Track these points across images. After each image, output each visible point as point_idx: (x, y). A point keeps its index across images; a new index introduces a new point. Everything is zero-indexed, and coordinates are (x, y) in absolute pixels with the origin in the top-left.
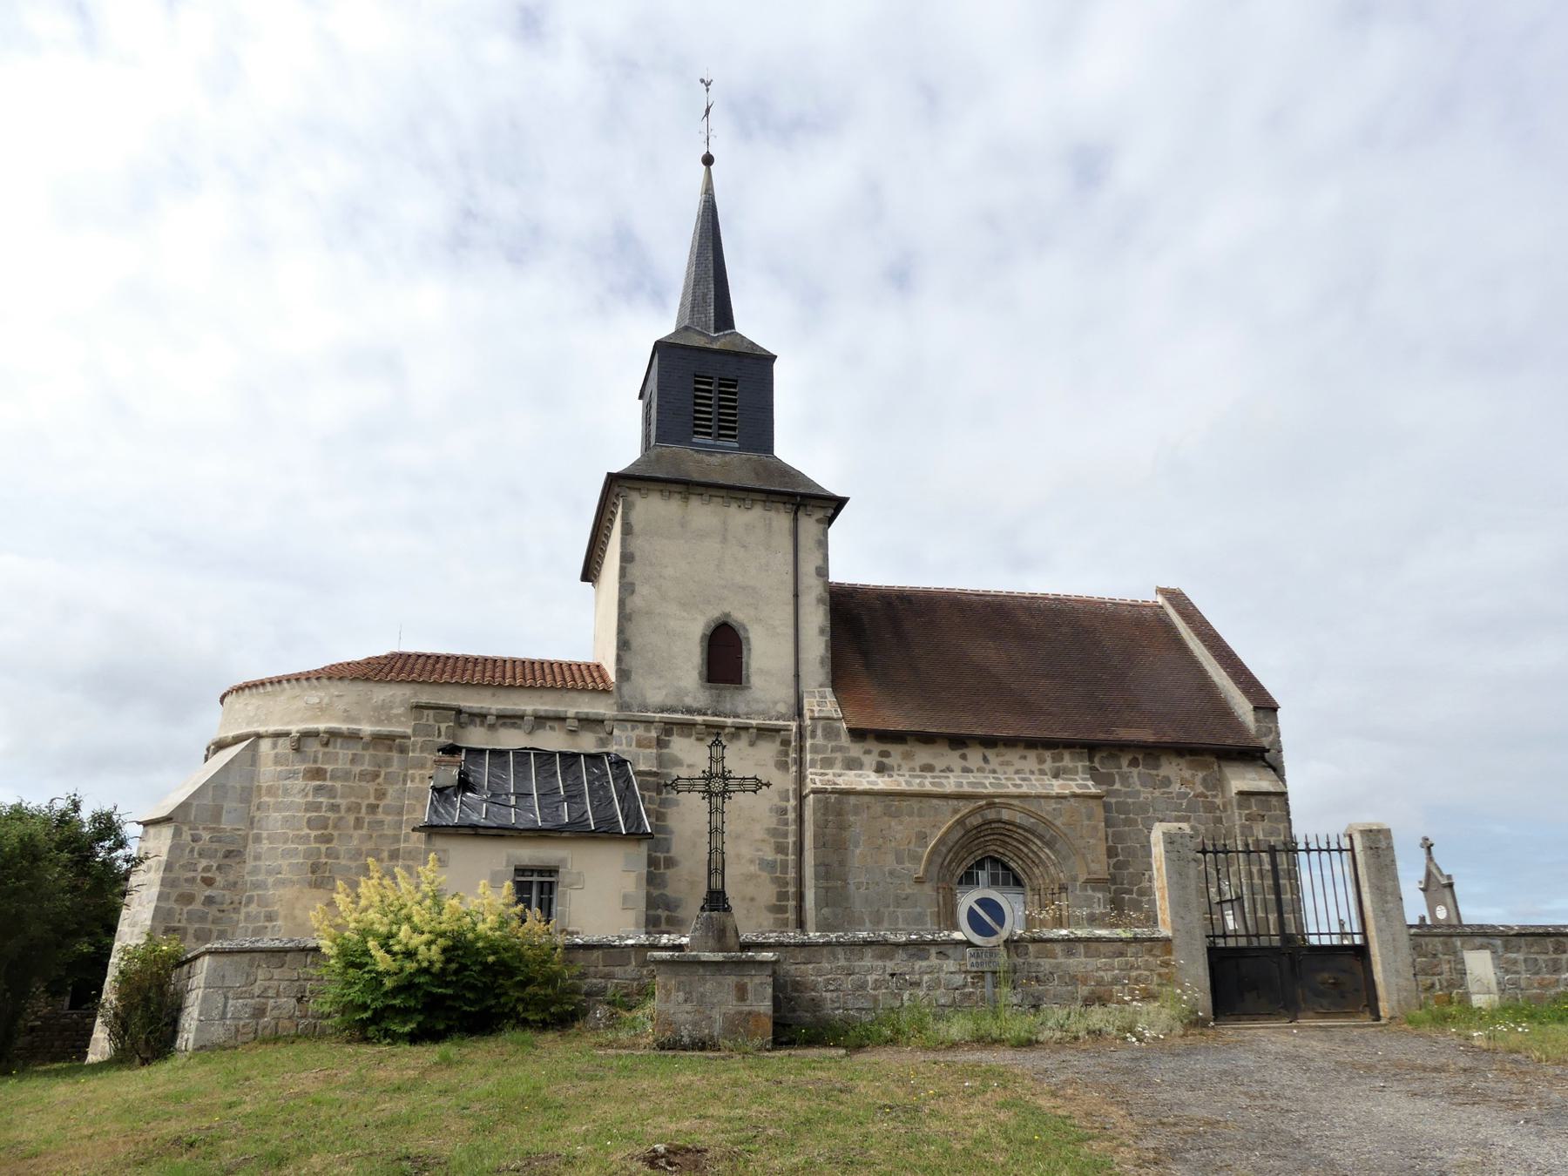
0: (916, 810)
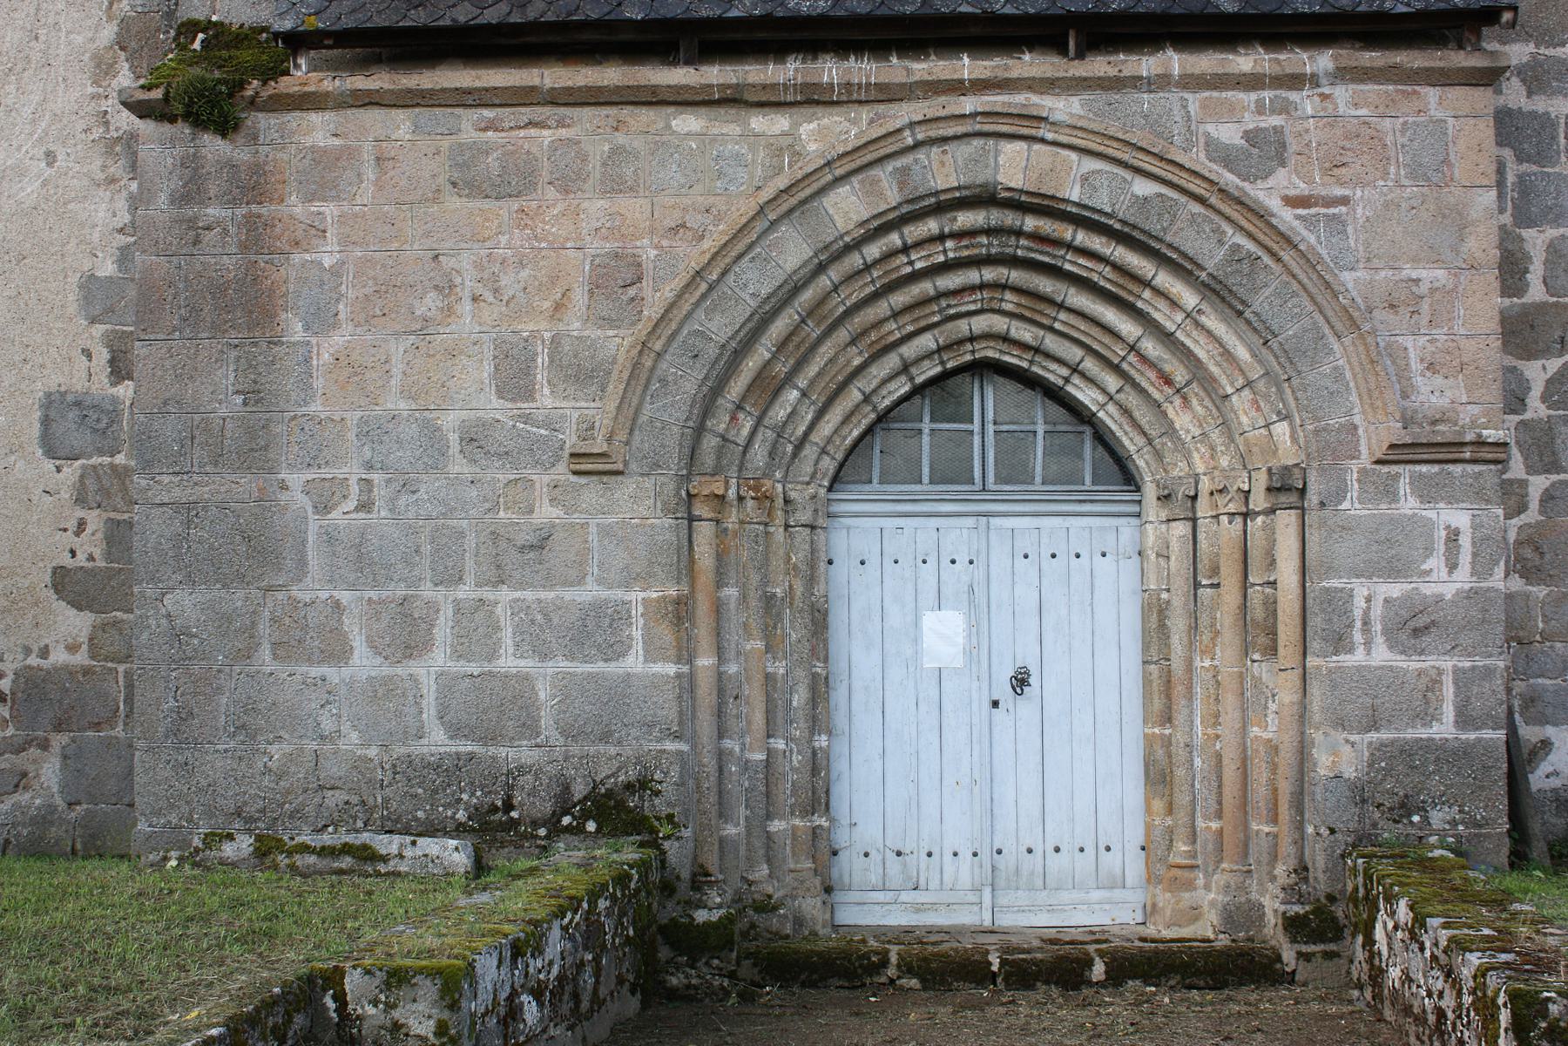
0: (594, 166)
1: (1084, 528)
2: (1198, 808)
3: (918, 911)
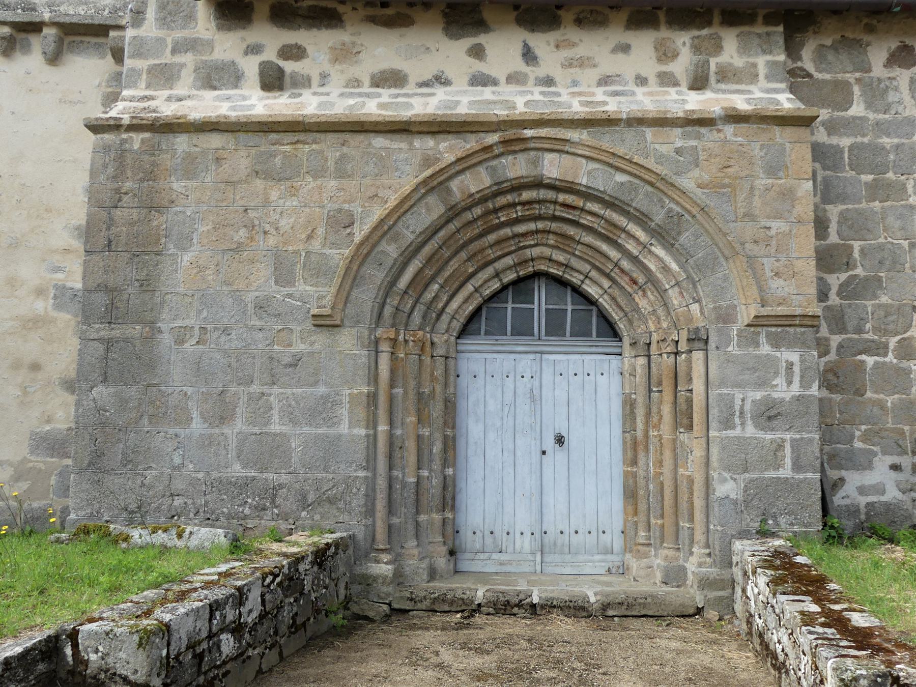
0: (331, 163)
1: (592, 360)
2: (651, 512)
3: (501, 564)
